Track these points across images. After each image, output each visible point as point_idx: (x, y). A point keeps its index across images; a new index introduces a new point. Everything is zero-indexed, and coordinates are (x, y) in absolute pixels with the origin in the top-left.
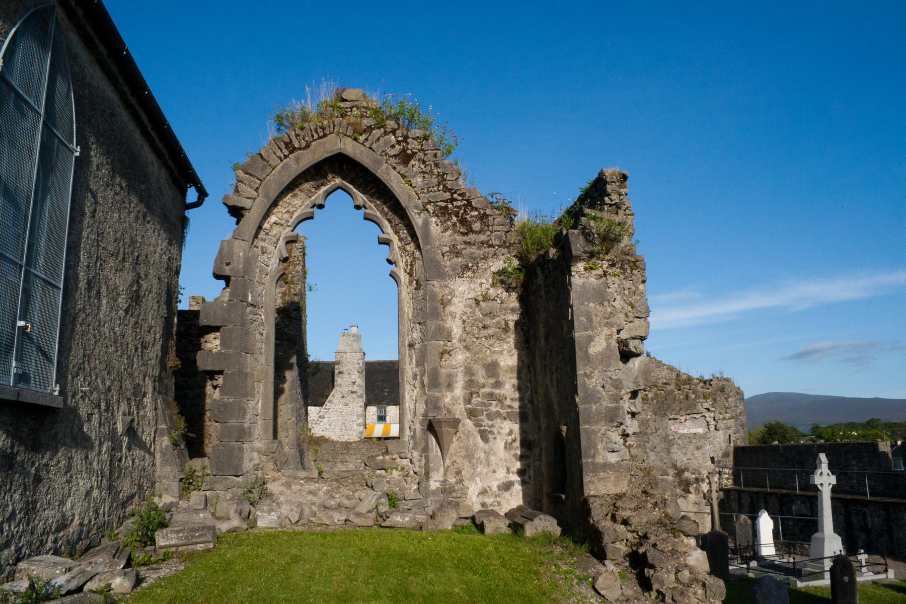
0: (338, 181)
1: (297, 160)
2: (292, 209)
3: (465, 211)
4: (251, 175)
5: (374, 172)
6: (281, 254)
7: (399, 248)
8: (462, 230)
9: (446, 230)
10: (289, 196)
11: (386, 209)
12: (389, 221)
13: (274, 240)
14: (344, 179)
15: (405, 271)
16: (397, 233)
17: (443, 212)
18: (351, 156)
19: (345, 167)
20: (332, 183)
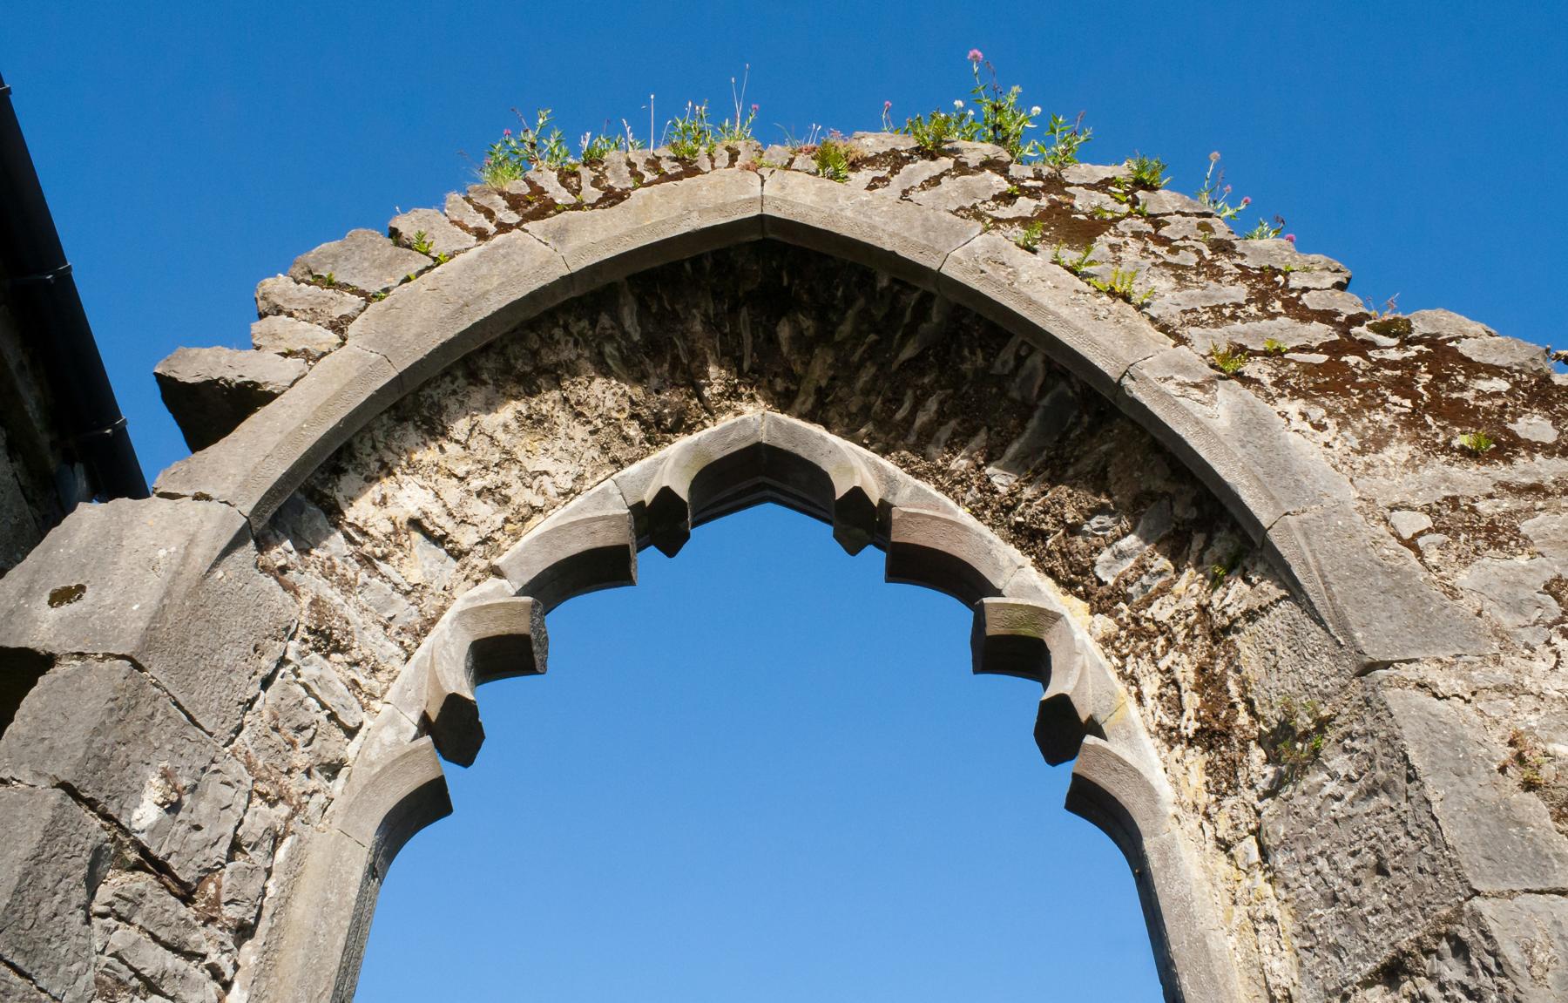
0: (753, 419)
1: (560, 235)
2: (521, 496)
3: (1439, 377)
4: (331, 284)
5: (932, 263)
6: (436, 682)
7: (1107, 641)
8: (1462, 440)
9: (1380, 441)
10: (508, 412)
11: (1002, 480)
12: (1027, 537)
13: (406, 612)
14: (784, 402)
15: (1171, 736)
16: (1076, 578)
17: (1331, 379)
18: (815, 221)
19: (784, 331)
20: (727, 420)
